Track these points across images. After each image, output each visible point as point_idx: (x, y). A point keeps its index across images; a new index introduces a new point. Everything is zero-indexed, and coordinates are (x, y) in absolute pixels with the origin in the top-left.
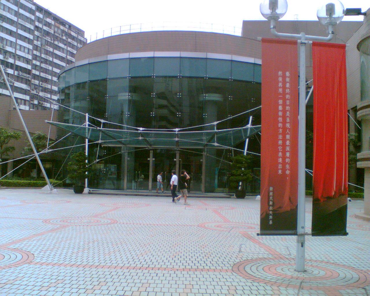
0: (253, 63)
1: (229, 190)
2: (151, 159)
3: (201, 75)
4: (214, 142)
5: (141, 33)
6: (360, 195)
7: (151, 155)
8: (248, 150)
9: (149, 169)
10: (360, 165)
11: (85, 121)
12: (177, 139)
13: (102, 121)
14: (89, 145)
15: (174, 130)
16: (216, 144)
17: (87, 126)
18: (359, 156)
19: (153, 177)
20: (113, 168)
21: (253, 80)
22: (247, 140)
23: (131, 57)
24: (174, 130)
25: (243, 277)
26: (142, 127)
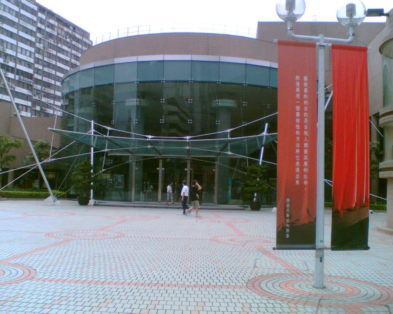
0: (269, 67)
1: (243, 201)
2: (161, 169)
3: (214, 79)
4: (227, 151)
5: (149, 35)
6: (382, 207)
7: (161, 164)
8: (263, 159)
9: (158, 179)
10: (382, 175)
11: (90, 129)
12: (188, 148)
13: (109, 128)
14: (94, 154)
15: (185, 138)
16: (229, 153)
17: (92, 134)
18: (382, 165)
19: (162, 188)
20: (120, 178)
21: (269, 85)
22: (263, 148)
23: (139, 60)
24: (185, 138)
25: (258, 294)
26: (151, 135)
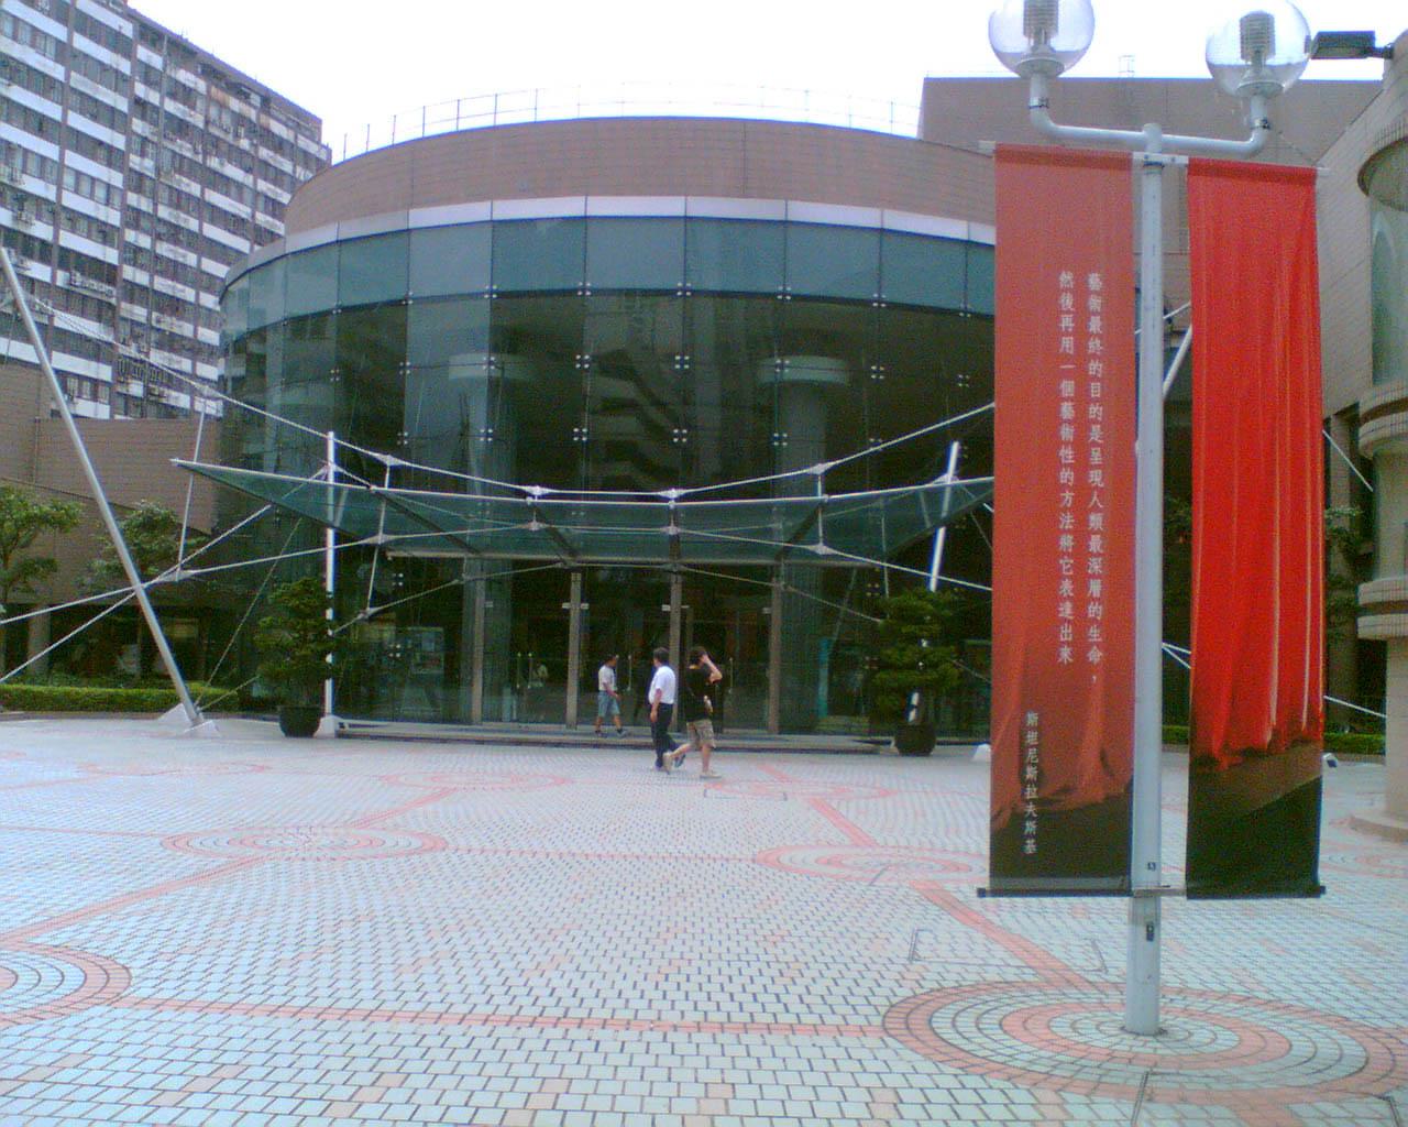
0: (962, 241)
1: (871, 722)
2: (575, 607)
3: (766, 284)
4: (815, 542)
5: (535, 124)
6: (1370, 742)
7: (576, 588)
8: (942, 571)
10: (1369, 627)
11: (323, 462)
12: (672, 530)
13: (390, 461)
14: (337, 553)
15: (662, 494)
16: (821, 549)
17: (331, 481)
18: (1367, 592)
20: (429, 639)
21: (962, 306)
22: (941, 532)
23: (498, 216)
24: (662, 494)
26: (542, 485)
